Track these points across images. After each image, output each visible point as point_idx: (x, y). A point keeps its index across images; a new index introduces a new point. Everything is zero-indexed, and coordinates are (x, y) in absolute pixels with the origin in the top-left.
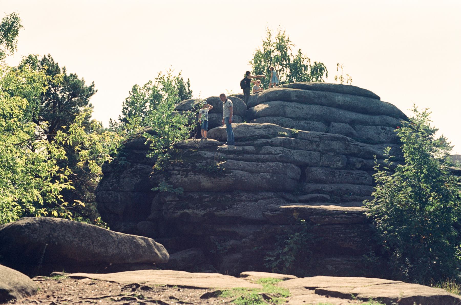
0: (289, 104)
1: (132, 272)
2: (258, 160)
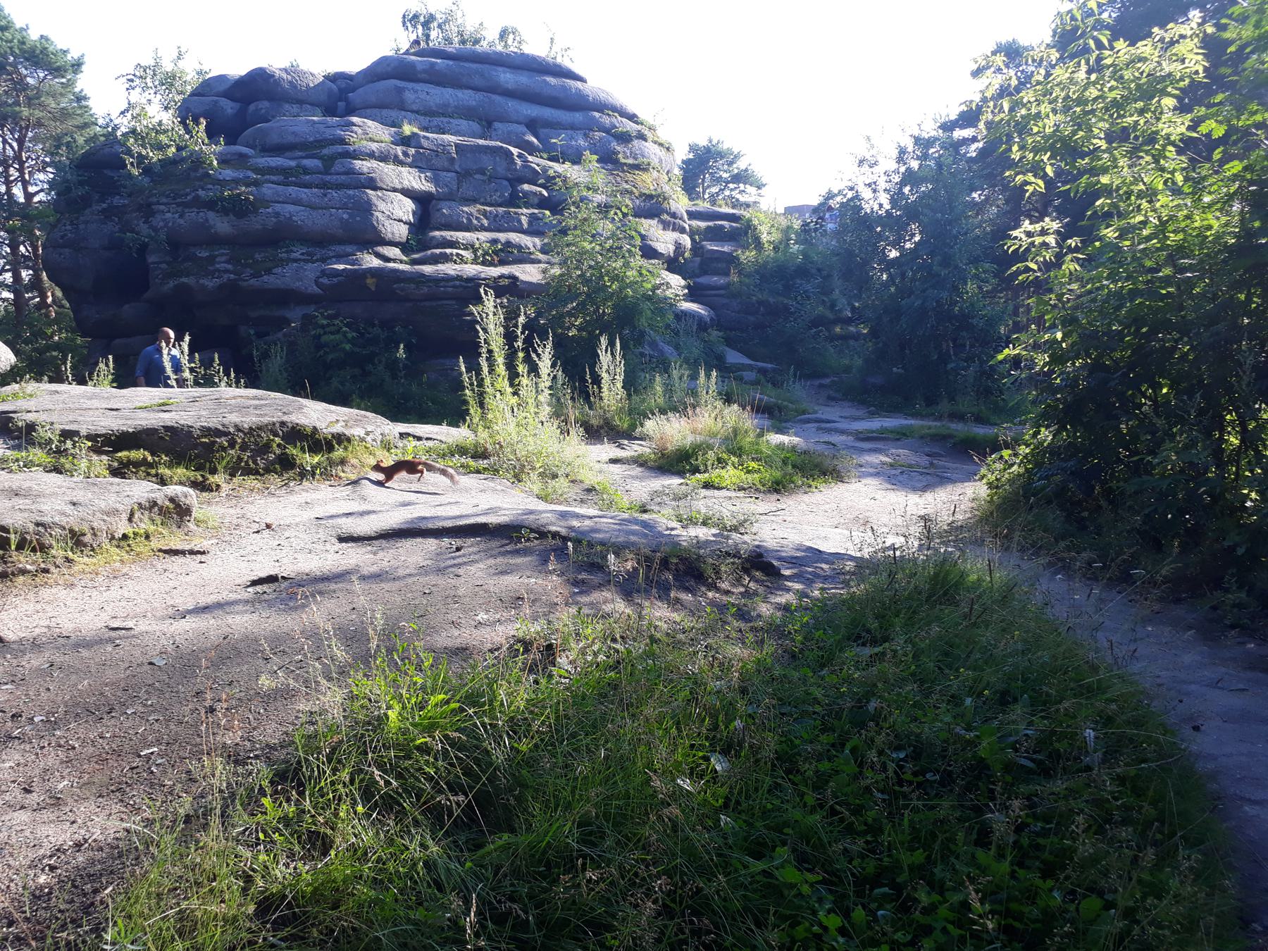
1: (333, 407)
2: (324, 186)
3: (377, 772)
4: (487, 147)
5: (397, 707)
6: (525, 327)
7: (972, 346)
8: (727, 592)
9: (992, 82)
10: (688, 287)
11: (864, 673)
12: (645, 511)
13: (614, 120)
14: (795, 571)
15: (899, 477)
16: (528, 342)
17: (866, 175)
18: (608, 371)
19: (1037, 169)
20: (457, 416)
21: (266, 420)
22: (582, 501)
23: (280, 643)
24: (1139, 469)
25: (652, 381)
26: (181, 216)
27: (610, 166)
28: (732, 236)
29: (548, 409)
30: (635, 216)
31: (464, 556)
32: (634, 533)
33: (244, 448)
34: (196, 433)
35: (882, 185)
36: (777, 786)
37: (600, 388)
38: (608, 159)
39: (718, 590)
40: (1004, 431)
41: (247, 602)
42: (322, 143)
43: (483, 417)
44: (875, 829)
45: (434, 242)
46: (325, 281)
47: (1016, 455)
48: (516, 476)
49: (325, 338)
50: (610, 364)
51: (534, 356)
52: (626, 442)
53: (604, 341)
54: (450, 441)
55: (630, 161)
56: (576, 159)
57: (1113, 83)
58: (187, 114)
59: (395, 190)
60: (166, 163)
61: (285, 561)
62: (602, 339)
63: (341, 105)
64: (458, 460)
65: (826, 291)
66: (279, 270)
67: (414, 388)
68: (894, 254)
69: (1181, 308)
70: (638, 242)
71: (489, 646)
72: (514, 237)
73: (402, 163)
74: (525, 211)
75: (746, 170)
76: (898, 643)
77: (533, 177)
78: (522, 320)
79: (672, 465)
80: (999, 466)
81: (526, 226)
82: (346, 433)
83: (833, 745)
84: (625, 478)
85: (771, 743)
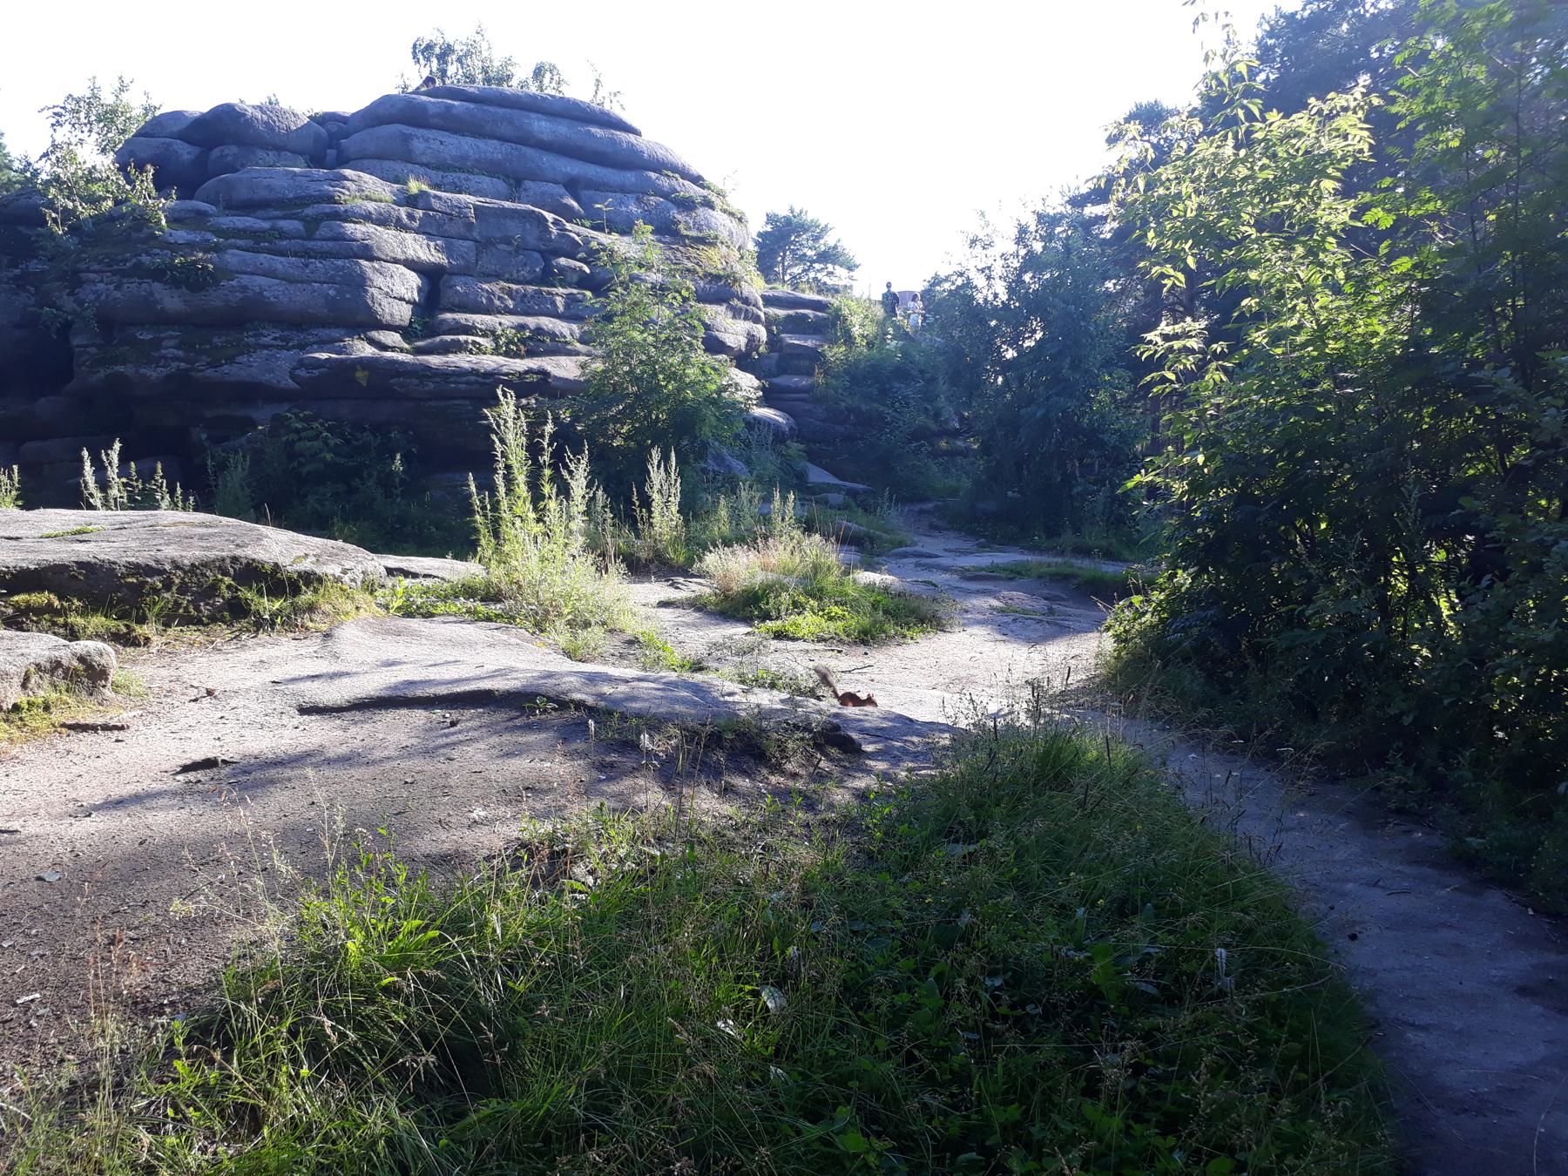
0: (421, 132)
1: (302, 537)
2: (306, 254)
3: (328, 1023)
4: (515, 211)
5: (360, 936)
6: (553, 437)
7: (1102, 466)
8: (794, 776)
9: (1130, 151)
10: (763, 389)
11: (954, 879)
12: (701, 669)
13: (674, 182)
14: (879, 746)
15: (1011, 625)
16: (558, 456)
17: (979, 258)
18: (660, 491)
19: (1175, 259)
20: (464, 546)
21: (212, 554)
22: (621, 656)
23: (206, 854)
24: (1294, 621)
25: (716, 503)
26: (117, 288)
27: (668, 238)
28: (817, 328)
29: (581, 539)
30: (698, 301)
31: (460, 732)
32: (683, 701)
33: (183, 590)
34: (120, 571)
35: (998, 270)
36: (844, 1027)
37: (650, 512)
38: (666, 230)
39: (783, 772)
40: (1136, 570)
41: (174, 794)
42: (304, 201)
43: (497, 549)
44: (962, 1078)
45: (445, 327)
46: (302, 373)
47: (1148, 601)
48: (537, 625)
49: (300, 446)
50: (663, 484)
51: (565, 473)
52: (681, 580)
53: (656, 454)
54: (455, 579)
55: (694, 233)
56: (625, 228)
57: (1265, 161)
58: (129, 160)
59: (396, 261)
60: (99, 220)
61: (228, 739)
62: (654, 452)
63: (331, 153)
64: (462, 604)
65: (929, 397)
66: (244, 359)
67: (414, 509)
68: (1010, 354)
69: (1342, 427)
70: (701, 333)
71: (486, 852)
72: (547, 323)
73: (406, 228)
74: (561, 290)
75: (835, 247)
76: (997, 840)
77: (571, 250)
78: (549, 428)
79: (737, 610)
80: (1128, 614)
81: (561, 309)
82: (318, 571)
83: (915, 971)
84: (677, 626)
85: (837, 969)
